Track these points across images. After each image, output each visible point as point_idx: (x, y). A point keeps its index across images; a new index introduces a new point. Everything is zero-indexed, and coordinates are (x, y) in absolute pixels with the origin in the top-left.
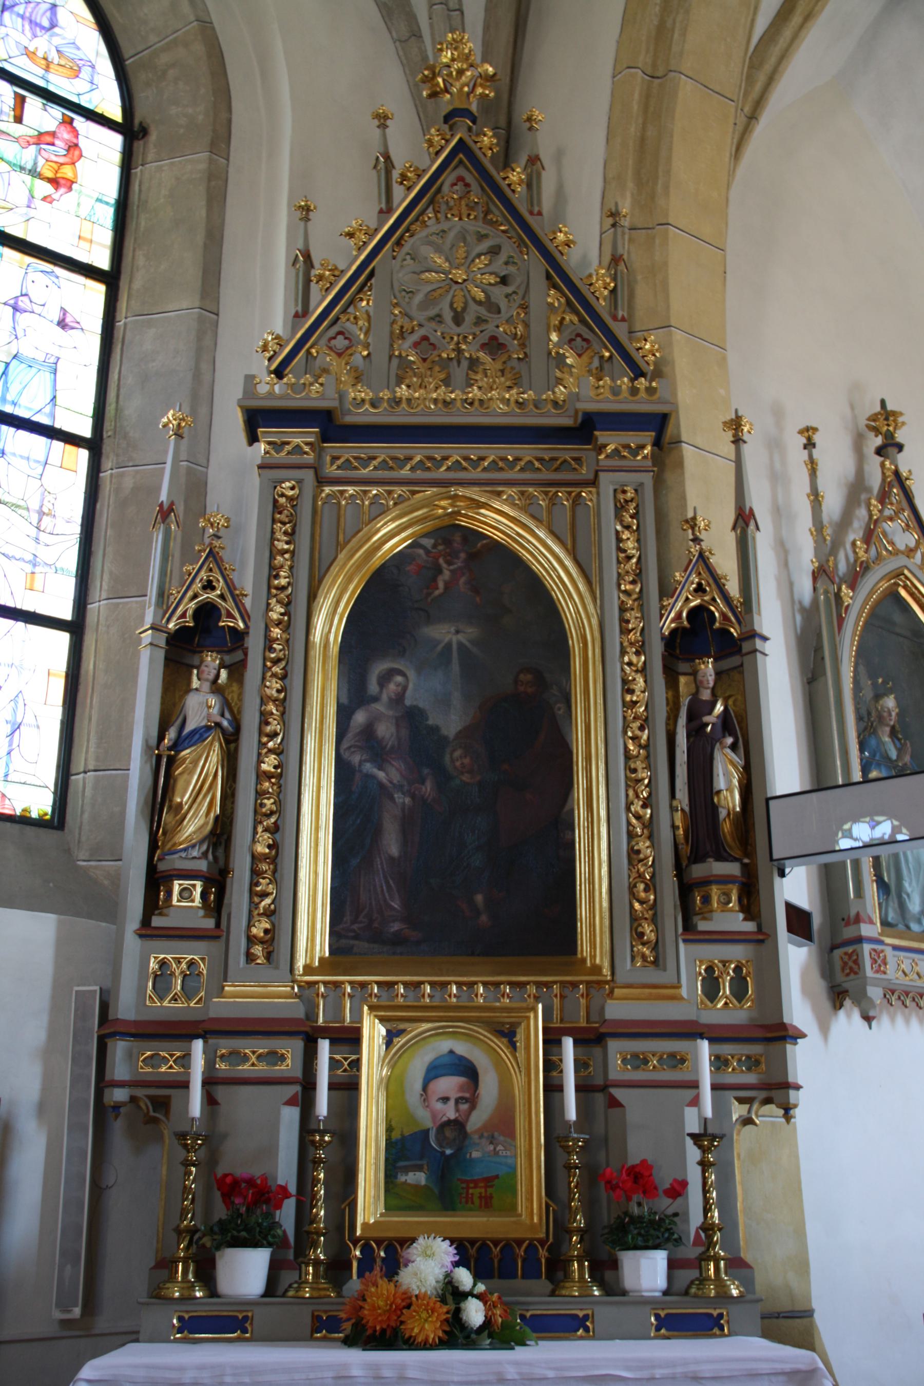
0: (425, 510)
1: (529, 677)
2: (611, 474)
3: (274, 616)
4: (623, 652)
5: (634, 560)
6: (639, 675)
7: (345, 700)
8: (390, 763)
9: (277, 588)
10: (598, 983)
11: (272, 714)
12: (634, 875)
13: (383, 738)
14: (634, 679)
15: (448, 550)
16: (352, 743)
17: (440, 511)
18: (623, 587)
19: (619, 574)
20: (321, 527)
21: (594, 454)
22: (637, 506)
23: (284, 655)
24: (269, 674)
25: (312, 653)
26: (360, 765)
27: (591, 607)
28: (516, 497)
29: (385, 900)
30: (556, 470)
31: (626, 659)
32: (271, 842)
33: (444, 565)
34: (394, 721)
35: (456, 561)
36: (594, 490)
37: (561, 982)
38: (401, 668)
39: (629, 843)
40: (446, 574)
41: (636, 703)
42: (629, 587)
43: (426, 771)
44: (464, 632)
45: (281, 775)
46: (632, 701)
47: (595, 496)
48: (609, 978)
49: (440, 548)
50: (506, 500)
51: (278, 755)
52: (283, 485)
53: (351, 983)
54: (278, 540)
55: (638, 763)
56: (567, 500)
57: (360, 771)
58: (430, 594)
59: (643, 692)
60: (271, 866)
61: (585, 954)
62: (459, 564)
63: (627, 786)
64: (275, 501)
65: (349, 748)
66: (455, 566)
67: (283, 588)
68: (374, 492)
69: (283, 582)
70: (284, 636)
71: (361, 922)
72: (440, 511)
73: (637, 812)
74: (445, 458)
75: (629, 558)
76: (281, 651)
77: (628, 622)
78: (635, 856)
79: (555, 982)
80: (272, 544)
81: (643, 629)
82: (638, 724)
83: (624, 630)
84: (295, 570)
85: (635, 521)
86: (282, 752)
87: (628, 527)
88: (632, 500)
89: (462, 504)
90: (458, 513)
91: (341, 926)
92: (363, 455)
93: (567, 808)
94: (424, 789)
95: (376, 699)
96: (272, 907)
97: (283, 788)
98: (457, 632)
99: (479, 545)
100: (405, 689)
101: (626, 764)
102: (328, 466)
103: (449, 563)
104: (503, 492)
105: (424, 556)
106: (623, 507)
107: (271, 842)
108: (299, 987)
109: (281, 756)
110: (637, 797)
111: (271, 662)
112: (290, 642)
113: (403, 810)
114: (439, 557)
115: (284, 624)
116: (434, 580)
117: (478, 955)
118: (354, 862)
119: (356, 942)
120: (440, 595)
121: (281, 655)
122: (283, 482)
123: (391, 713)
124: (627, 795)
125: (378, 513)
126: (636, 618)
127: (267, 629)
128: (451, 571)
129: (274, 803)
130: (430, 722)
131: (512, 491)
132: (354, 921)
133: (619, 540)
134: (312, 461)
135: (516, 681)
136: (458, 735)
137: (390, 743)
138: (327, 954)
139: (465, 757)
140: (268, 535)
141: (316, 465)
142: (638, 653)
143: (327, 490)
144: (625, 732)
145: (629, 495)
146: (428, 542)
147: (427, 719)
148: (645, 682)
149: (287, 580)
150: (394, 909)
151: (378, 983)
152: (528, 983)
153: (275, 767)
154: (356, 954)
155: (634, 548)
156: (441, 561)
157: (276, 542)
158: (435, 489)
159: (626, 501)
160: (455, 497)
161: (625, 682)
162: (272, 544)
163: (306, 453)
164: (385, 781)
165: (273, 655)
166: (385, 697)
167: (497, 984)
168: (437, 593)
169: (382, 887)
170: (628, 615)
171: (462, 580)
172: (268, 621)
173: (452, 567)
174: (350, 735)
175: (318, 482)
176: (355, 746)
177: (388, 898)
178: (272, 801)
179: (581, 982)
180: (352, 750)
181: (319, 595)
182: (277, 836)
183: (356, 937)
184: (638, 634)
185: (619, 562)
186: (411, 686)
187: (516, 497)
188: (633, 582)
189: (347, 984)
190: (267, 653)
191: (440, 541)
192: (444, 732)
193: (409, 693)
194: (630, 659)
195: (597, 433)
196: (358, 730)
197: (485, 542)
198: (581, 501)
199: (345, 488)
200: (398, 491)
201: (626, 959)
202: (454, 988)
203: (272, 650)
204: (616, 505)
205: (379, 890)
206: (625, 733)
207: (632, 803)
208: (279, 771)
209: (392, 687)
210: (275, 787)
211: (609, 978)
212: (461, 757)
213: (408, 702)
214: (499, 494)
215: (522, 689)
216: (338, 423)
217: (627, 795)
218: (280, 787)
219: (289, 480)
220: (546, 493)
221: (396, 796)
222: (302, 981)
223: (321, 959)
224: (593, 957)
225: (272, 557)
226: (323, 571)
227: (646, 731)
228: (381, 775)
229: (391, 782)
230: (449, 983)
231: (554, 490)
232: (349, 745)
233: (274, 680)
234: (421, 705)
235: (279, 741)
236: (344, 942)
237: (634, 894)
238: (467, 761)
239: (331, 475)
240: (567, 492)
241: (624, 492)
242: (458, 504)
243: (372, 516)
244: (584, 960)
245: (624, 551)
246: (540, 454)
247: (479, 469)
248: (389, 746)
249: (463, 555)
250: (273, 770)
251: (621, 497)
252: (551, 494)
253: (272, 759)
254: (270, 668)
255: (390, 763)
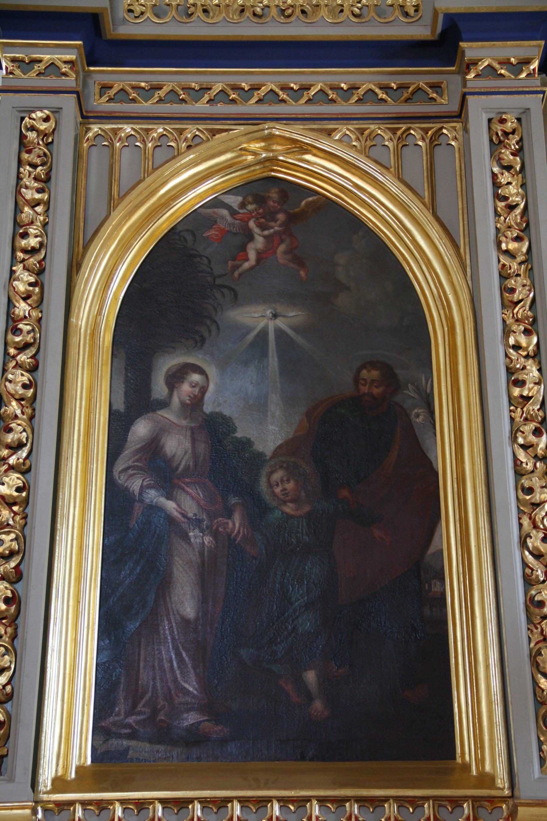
0: (228, 156)
1: (375, 374)
2: (484, 97)
3: (21, 287)
4: (507, 332)
5: (518, 211)
6: (530, 361)
7: (120, 406)
8: (184, 490)
9: (25, 251)
10: (491, 799)
11: (16, 417)
12: (537, 637)
13: (174, 456)
14: (524, 368)
15: (261, 211)
16: (130, 463)
17: (250, 158)
18: (504, 246)
19: (498, 230)
20: (86, 177)
21: (458, 78)
22: (521, 139)
23: (35, 339)
24: (13, 363)
25: (73, 341)
26: (140, 494)
27: (458, 278)
28: (353, 137)
29: (175, 680)
30: (407, 100)
31: (512, 341)
32: (9, 594)
33: (256, 230)
34: (189, 433)
35: (272, 224)
36: (458, 125)
37: (435, 798)
38: (198, 363)
39: (526, 593)
40: (259, 242)
41: (528, 398)
42: (512, 246)
43: (234, 500)
44: (284, 316)
45: (26, 501)
46: (522, 396)
47: (461, 133)
48: (507, 792)
49: (250, 207)
50: (340, 141)
51: (23, 473)
52: (33, 115)
53: (122, 802)
54: (27, 187)
55: (535, 479)
56: (423, 139)
57: (141, 501)
58: (238, 267)
59: (538, 383)
60: (9, 630)
61: (467, 758)
62: (277, 228)
63: (520, 512)
64: (22, 137)
65: (126, 469)
66: (272, 231)
67: (33, 251)
68: (160, 130)
69: (33, 242)
70: (34, 314)
71: (140, 713)
72: (250, 158)
73: (536, 548)
74: (255, 88)
75: (511, 208)
76: (29, 332)
77: (512, 291)
78: (537, 611)
79: (426, 798)
80: (18, 192)
81: (534, 300)
82: (532, 426)
83: (506, 302)
84: (50, 228)
85: (518, 159)
86: (29, 470)
87: (509, 168)
88: (513, 132)
89: (279, 148)
90: (273, 160)
91: (111, 719)
92: (143, 84)
93: (432, 549)
94: (230, 524)
95: (164, 404)
96: (8, 688)
97: (29, 519)
98: (275, 316)
99: (303, 203)
100: (204, 390)
101: (517, 482)
102: (97, 97)
103: (263, 227)
104: (335, 130)
105: (229, 218)
106: (500, 142)
107: (9, 594)
108: (45, 810)
109: (27, 476)
110: (535, 527)
111: (15, 348)
112: (43, 322)
113: (202, 554)
114: (249, 219)
115: (34, 298)
116: (243, 248)
117: (311, 760)
118: (132, 626)
119: (133, 743)
120: (252, 268)
121: (29, 338)
122: (34, 112)
123: (184, 423)
124: (521, 525)
125: (165, 160)
126: (524, 286)
127: (10, 304)
128: (265, 237)
129: (16, 539)
130: (239, 434)
131: (344, 129)
132: (131, 712)
133: (496, 185)
134: (73, 84)
135: (357, 380)
136: (276, 453)
137: (183, 463)
138: (89, 762)
139: (288, 481)
140: (13, 181)
141: (79, 89)
142: (527, 332)
143: (95, 128)
144: (514, 439)
145: (509, 126)
146: (234, 201)
147: (235, 430)
148: (540, 370)
149: (39, 239)
150: (188, 692)
151: (162, 801)
152: (386, 799)
153: (18, 490)
154: (132, 760)
155: (517, 194)
156: (252, 224)
157: (23, 190)
158: (242, 128)
159: (506, 134)
160: (269, 138)
161: (510, 371)
162: (18, 192)
163: (65, 74)
164: (176, 514)
165: (17, 339)
166: (176, 400)
167: (340, 802)
168: (246, 265)
169: (171, 661)
170: (511, 283)
171: (282, 248)
172: (12, 293)
173: (266, 233)
174: (127, 452)
175: (83, 117)
176: (134, 467)
177: (179, 676)
178: (13, 536)
179: (466, 798)
180: (131, 472)
181: (84, 266)
182: (19, 587)
183: (133, 736)
184: (527, 308)
185: (497, 214)
186: (212, 387)
187: (353, 137)
188: (518, 239)
189: (117, 805)
190: (10, 336)
191: (250, 199)
192: (259, 447)
193: (208, 396)
194: (516, 341)
195: (461, 44)
196: (139, 446)
197: (310, 199)
198: (442, 139)
199: (120, 126)
200: (191, 130)
201: (532, 762)
202: (276, 807)
203: (16, 331)
204: (491, 140)
205: (166, 665)
206: (514, 439)
207: (529, 536)
208: (24, 494)
209: (186, 388)
210: (18, 518)
211: (507, 792)
212: (282, 481)
213: (208, 408)
214: (329, 133)
215: (365, 389)
216: (109, 37)
217: (521, 525)
218: (25, 518)
219: (41, 109)
220: (394, 131)
221: (191, 534)
222: (49, 802)
223: (79, 769)
224: (481, 761)
225: (18, 210)
226: (88, 237)
227: (544, 437)
228: (170, 505)
229: (184, 516)
230: (269, 800)
231: (404, 127)
232: (126, 465)
233: (19, 372)
234: (226, 412)
235: (24, 455)
236: (115, 743)
237: (538, 665)
238: (290, 486)
239: (100, 108)
240: (422, 129)
241: (503, 121)
242: (275, 147)
243: (157, 163)
244: (466, 767)
245: (506, 198)
246: (384, 80)
247: (303, 101)
248: (181, 468)
249: (281, 217)
250: (15, 494)
251: (498, 128)
252: (399, 133)
253: (15, 479)
254: (14, 357)
255: (184, 490)
